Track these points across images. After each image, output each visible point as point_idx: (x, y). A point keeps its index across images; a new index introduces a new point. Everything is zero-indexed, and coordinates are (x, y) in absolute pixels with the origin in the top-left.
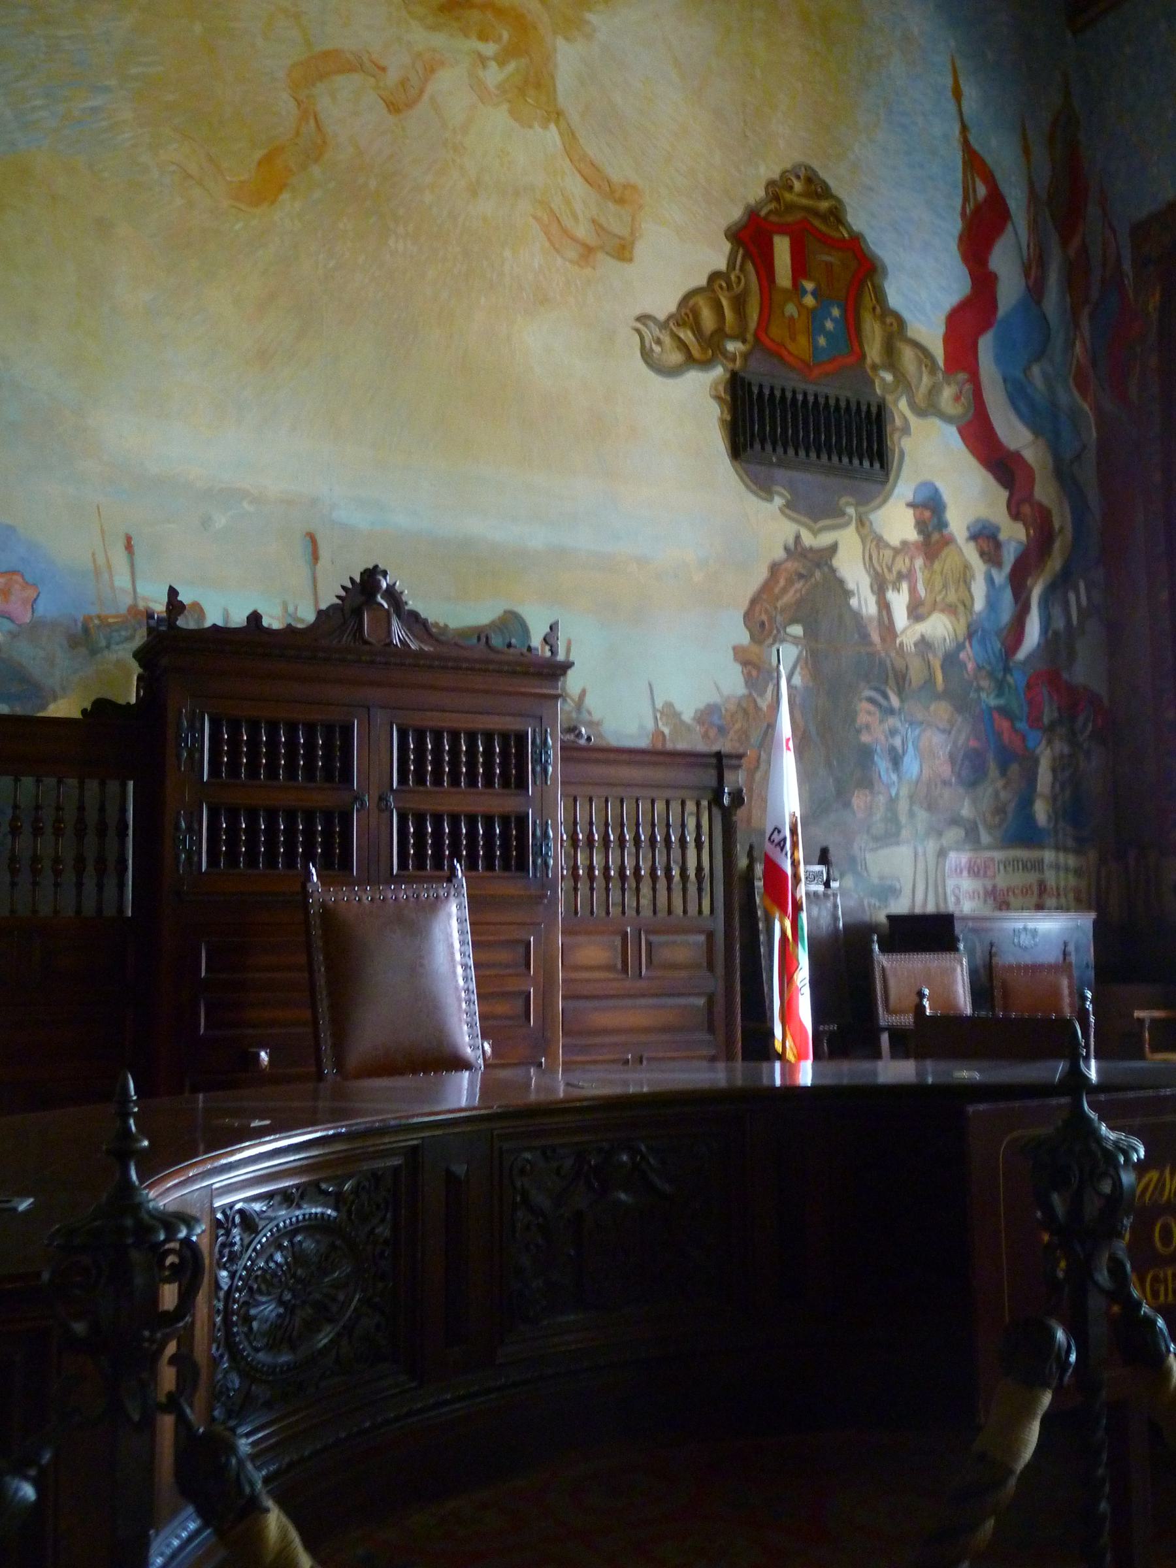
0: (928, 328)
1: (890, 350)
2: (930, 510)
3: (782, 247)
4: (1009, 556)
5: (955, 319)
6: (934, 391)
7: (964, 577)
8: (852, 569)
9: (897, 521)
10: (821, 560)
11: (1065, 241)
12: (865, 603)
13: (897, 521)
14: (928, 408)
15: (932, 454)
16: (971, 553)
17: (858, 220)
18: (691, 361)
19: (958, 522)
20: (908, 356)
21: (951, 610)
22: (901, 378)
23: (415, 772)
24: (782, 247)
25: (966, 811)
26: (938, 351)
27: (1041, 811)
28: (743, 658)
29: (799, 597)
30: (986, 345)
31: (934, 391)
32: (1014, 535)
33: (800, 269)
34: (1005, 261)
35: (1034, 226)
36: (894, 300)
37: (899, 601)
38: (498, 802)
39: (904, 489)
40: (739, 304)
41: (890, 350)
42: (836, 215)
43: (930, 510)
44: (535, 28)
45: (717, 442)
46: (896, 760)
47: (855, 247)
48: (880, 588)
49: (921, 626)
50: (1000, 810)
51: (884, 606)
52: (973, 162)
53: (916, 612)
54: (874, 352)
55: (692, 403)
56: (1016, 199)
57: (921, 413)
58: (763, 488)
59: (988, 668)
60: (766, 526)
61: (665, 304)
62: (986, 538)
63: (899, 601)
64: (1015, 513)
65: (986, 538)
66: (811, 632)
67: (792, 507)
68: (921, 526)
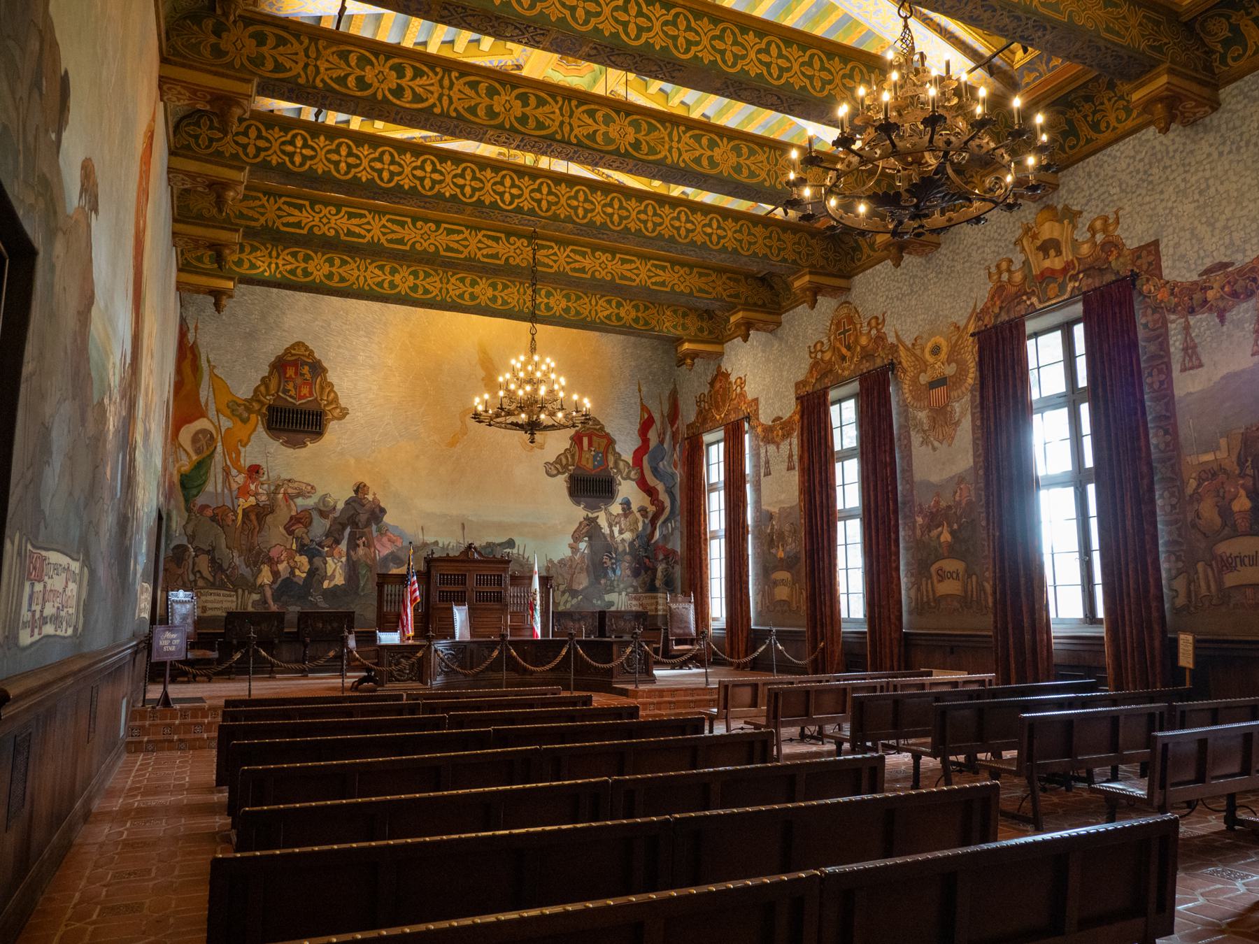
0: (628, 457)
1: (616, 463)
2: (627, 504)
3: (585, 440)
4: (650, 515)
5: (636, 452)
6: (629, 472)
7: (636, 522)
8: (603, 522)
9: (616, 508)
10: (595, 520)
11: (672, 426)
12: (606, 530)
13: (616, 508)
14: (628, 478)
15: (627, 489)
16: (638, 515)
17: (608, 430)
18: (559, 473)
19: (634, 507)
20: (621, 464)
21: (631, 531)
22: (620, 472)
23: (479, 583)
24: (585, 440)
25: (635, 584)
26: (631, 462)
27: (658, 583)
28: (571, 547)
29: (590, 529)
30: (645, 459)
31: (629, 472)
32: (652, 509)
33: (590, 444)
34: (652, 435)
35: (662, 423)
36: (617, 449)
37: (616, 530)
38: (497, 589)
39: (619, 499)
40: (573, 456)
41: (616, 463)
42: (602, 428)
43: (627, 504)
44: (320, 18)
45: (565, 493)
46: (614, 571)
47: (607, 436)
48: (610, 526)
49: (623, 536)
50: (645, 583)
51: (612, 531)
52: (644, 408)
53: (621, 532)
54: (611, 464)
55: (560, 483)
56: (657, 416)
57: (624, 479)
58: (578, 503)
59: (385, 539)
60: (580, 513)
61: (552, 459)
62: (643, 511)
63: (616, 530)
64: (652, 504)
65: (643, 511)
66: (590, 538)
67: (587, 507)
68: (623, 509)
